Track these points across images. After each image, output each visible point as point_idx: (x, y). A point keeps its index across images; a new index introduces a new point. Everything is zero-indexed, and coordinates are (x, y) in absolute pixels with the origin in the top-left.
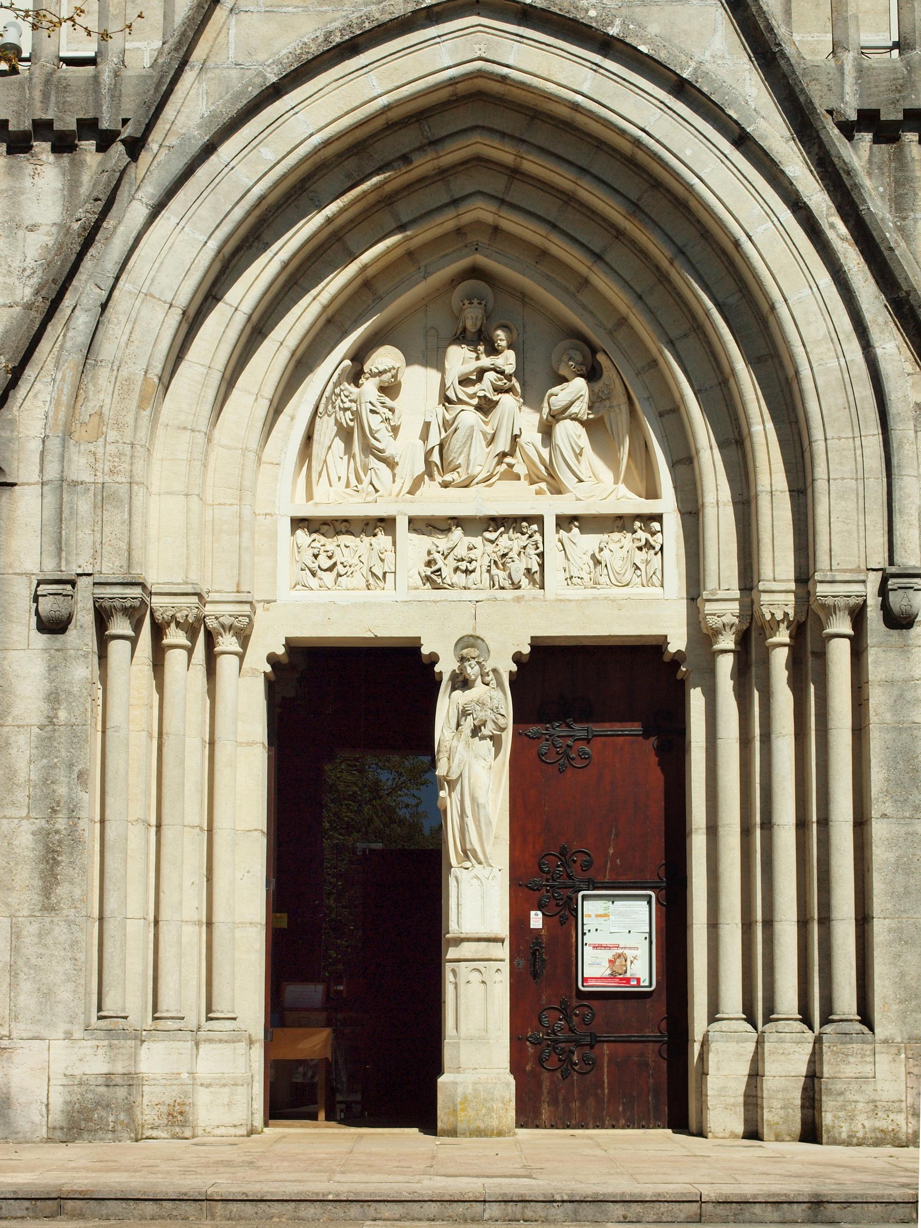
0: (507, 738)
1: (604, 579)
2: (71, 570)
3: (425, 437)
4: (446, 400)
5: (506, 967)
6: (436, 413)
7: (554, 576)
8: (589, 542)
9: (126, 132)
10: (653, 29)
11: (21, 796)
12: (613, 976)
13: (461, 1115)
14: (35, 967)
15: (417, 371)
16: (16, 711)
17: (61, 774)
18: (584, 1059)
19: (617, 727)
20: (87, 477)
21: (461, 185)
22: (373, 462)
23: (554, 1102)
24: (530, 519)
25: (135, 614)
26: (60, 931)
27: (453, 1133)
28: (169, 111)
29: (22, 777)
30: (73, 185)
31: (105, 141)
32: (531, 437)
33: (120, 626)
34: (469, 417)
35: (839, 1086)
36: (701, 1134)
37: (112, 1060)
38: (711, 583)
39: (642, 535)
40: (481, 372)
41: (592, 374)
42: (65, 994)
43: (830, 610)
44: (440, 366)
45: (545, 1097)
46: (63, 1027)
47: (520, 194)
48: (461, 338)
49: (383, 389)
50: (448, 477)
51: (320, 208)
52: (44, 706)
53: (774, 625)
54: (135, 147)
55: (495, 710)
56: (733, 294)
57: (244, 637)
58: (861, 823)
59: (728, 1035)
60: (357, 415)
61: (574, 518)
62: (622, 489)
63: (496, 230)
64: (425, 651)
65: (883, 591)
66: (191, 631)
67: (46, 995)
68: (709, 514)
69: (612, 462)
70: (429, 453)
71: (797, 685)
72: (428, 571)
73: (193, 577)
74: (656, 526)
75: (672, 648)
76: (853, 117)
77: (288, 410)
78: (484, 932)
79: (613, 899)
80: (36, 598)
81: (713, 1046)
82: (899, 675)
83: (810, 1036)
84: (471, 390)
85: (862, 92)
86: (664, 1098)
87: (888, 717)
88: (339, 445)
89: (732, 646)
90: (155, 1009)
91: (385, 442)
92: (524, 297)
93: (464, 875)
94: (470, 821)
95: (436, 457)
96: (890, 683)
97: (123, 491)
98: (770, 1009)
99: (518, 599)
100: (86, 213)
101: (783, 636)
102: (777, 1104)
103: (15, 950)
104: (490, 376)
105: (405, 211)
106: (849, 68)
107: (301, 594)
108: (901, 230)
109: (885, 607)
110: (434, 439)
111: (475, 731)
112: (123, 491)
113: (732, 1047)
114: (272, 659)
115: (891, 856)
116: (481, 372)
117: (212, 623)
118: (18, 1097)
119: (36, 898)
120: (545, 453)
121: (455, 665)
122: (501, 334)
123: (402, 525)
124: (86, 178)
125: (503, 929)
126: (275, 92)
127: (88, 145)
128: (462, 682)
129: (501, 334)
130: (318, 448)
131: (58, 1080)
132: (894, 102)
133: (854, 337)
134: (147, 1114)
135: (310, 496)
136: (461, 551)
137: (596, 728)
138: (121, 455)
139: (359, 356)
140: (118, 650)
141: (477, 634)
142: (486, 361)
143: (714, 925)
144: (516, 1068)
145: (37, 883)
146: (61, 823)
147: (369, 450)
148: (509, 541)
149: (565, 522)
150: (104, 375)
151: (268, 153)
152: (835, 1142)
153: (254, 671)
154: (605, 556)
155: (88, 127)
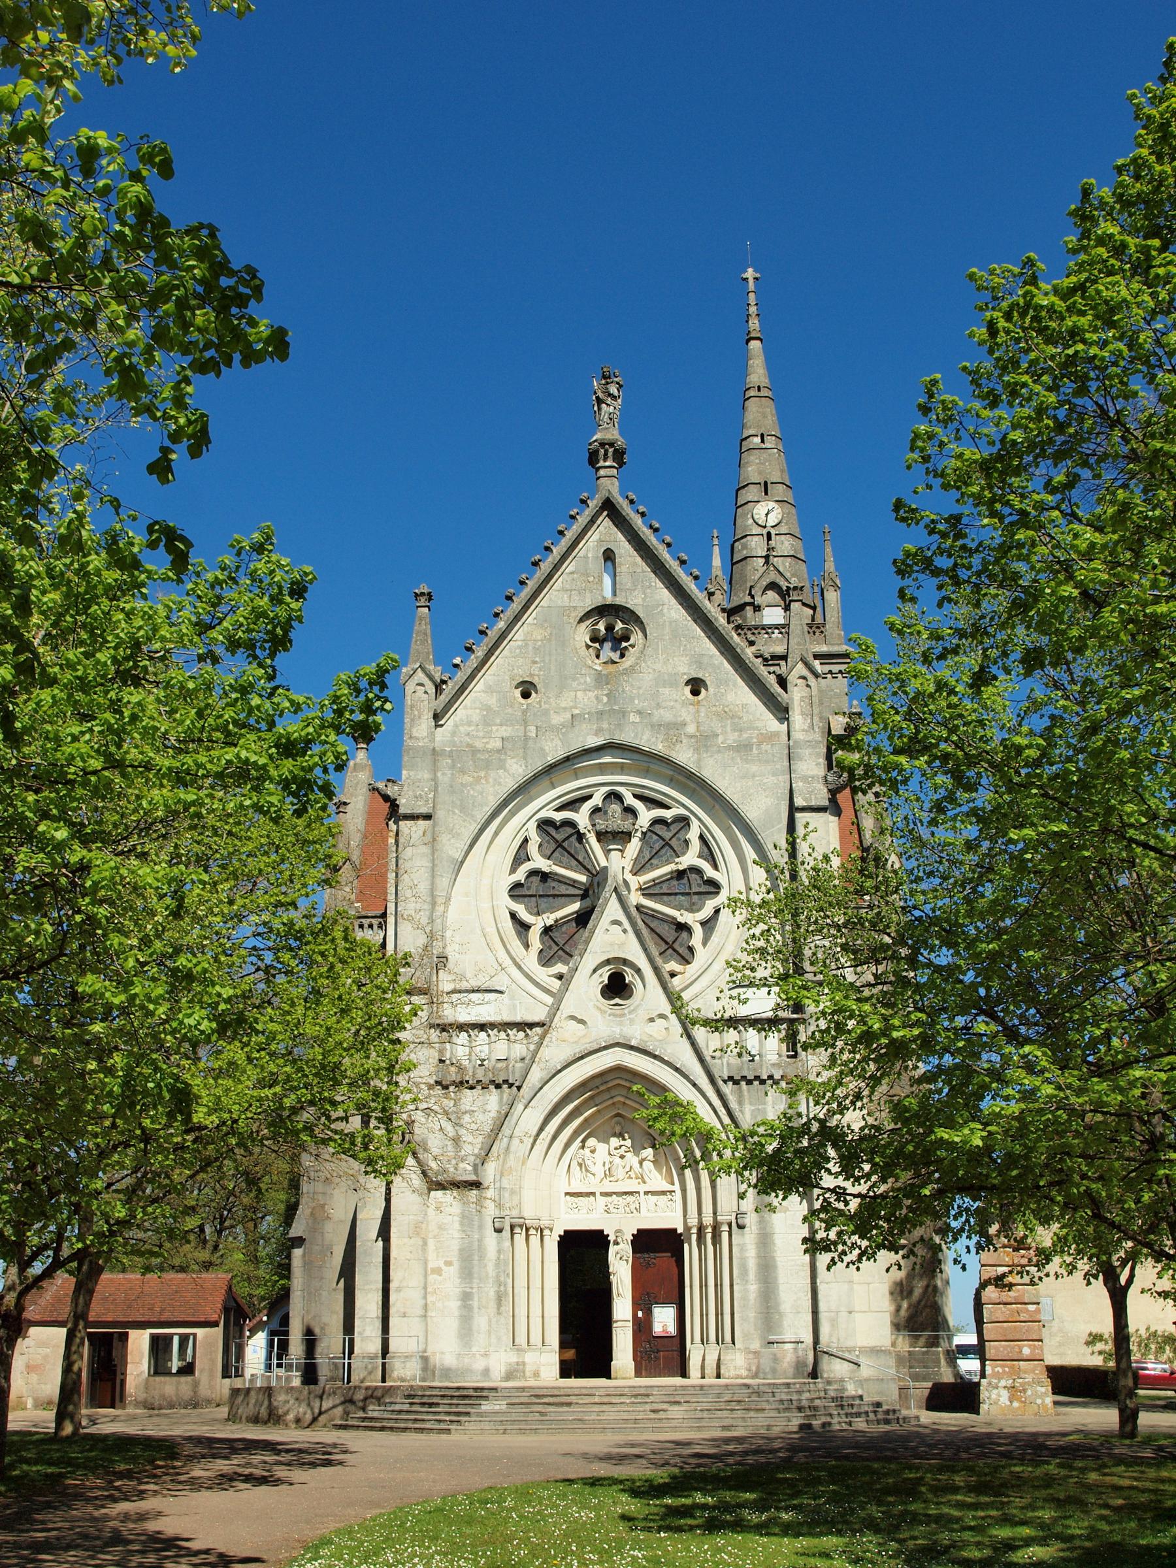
2: (503, 1214)
8: (655, 1198)
21: (613, 1093)
25: (521, 1226)
30: (501, 1099)
32: (636, 1165)
33: (517, 1230)
34: (617, 1160)
41: (653, 1147)
48: (614, 1135)
58: (732, 1286)
67: (499, 1339)
91: (592, 1169)
100: (505, 1108)
105: (598, 1100)
125: (630, 1317)
126: (560, 1071)
128: (616, 1243)
139: (583, 1141)
141: (619, 600)
144: (635, 1359)
148: (629, 1199)
149: (646, 1193)
150: (512, 1156)
151: (558, 1089)
155: (506, 1082)
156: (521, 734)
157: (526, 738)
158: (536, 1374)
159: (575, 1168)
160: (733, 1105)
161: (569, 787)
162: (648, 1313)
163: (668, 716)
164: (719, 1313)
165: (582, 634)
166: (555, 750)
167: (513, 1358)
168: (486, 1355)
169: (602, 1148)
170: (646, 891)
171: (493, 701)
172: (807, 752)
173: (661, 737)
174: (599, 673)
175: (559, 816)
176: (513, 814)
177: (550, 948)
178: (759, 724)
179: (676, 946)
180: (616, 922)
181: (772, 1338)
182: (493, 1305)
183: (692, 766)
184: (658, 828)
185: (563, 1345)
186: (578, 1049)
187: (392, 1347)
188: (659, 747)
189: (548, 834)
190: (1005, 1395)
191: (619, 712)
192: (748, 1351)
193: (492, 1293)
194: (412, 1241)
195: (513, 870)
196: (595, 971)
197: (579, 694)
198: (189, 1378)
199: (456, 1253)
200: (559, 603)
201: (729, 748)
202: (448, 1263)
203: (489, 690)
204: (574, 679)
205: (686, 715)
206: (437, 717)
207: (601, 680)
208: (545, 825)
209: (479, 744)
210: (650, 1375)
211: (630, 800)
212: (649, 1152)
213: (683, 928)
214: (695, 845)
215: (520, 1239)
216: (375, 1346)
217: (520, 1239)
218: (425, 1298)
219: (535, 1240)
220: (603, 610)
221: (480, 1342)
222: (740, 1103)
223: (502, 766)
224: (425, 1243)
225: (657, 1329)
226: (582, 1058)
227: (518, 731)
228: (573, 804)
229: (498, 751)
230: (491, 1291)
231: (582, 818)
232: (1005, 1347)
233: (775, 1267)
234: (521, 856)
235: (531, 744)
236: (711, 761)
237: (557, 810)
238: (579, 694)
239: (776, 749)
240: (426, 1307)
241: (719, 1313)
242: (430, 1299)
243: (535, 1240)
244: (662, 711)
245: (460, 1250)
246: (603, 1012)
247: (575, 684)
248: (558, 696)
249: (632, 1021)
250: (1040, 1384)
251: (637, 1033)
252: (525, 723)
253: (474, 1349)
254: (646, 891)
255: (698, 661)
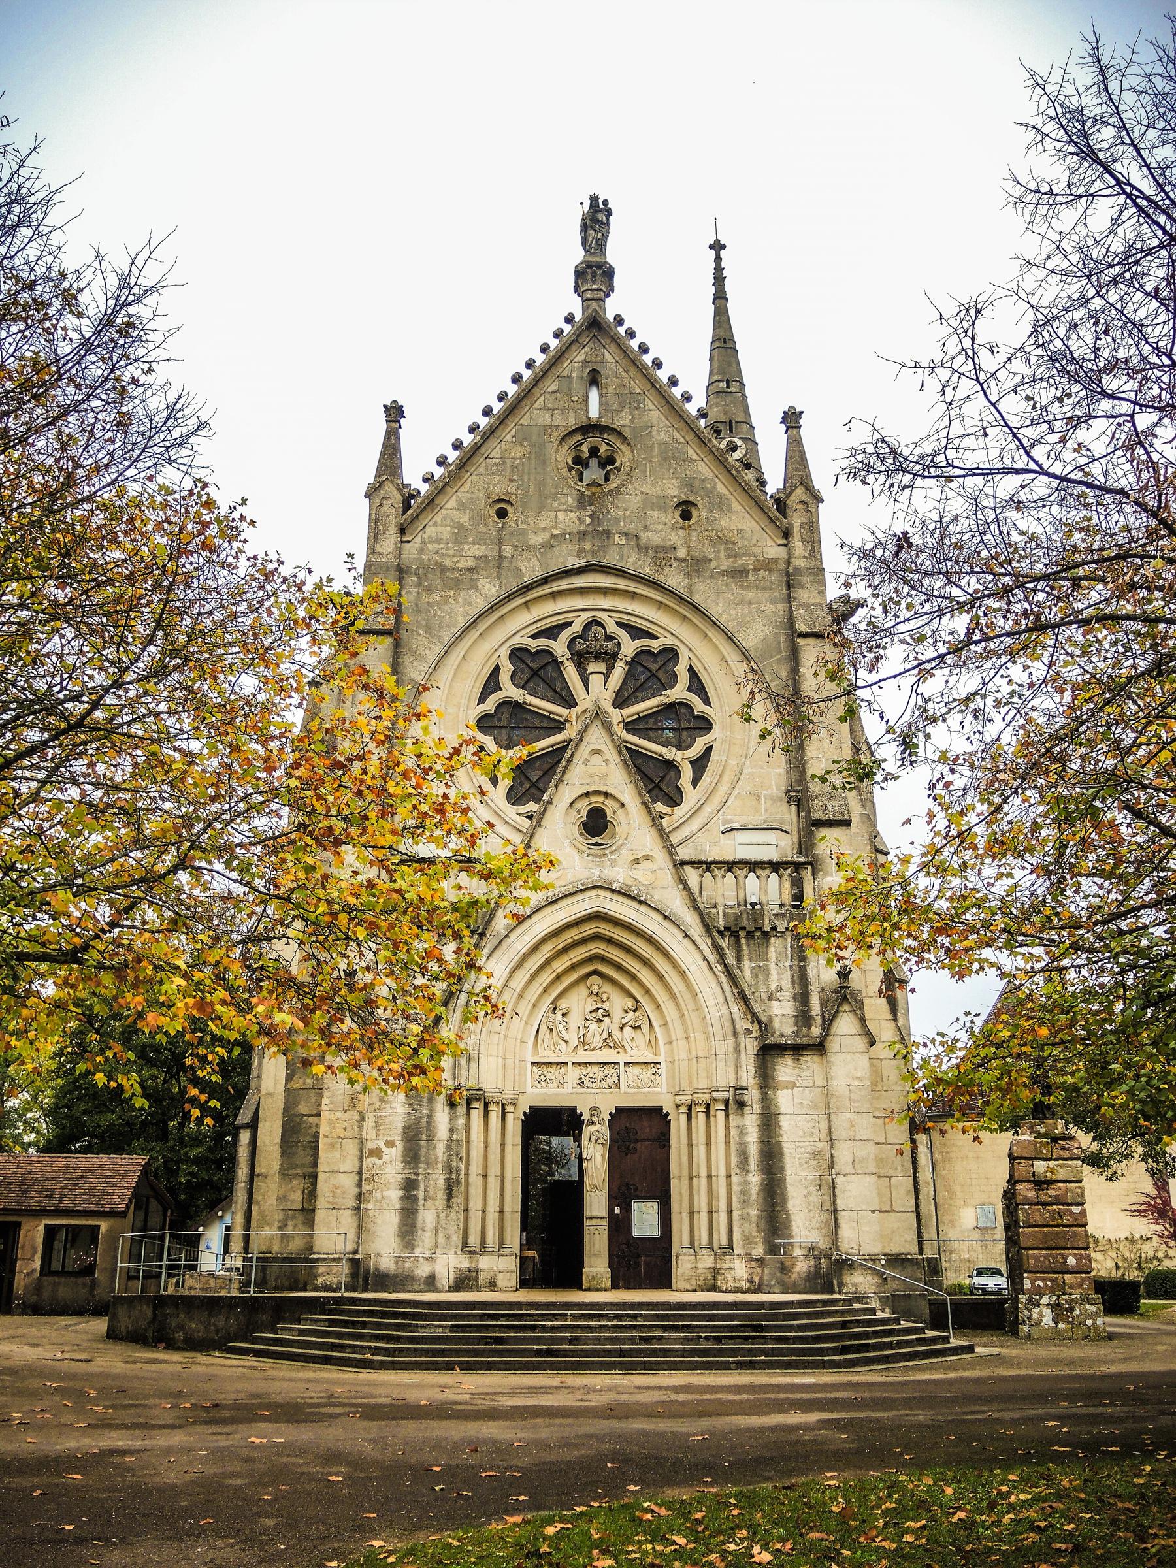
5: (607, 1232)
6: (581, 1024)
11: (440, 1166)
17: (454, 1158)
26: (453, 1215)
34: (593, 1026)
40: (598, 1009)
67: (448, 1238)
73: (499, 1086)
78: (600, 1215)
104: (601, 1011)
107: (533, 1090)
108: (739, 968)
115: (739, 1189)
116: (598, 1009)
123: (570, 1064)
125: (605, 1213)
131: (452, 1269)
133: (425, 1423)
134: (482, 1283)
136: (591, 1075)
146: (454, 1176)
148: (608, 1070)
151: (527, 938)
156: (495, 553)
157: (501, 557)
160: (731, 960)
161: (546, 611)
162: (628, 1210)
163: (656, 540)
165: (564, 456)
166: (531, 569)
167: (465, 1263)
168: (431, 1259)
171: (465, 519)
172: (809, 579)
173: (649, 560)
174: (582, 494)
175: (534, 645)
177: (521, 784)
178: (755, 550)
179: (662, 785)
180: (597, 752)
182: (441, 1195)
184: (643, 659)
185: (527, 1244)
189: (523, 661)
190: (1048, 1315)
191: (602, 533)
192: (749, 1258)
193: (441, 1182)
194: (347, 1116)
195: (482, 700)
196: (571, 804)
197: (560, 514)
198: (88, 1279)
199: (400, 1131)
200: (541, 422)
201: (724, 573)
202: (390, 1144)
204: (555, 499)
205: (676, 538)
206: (402, 531)
207: (583, 501)
208: (518, 654)
209: (448, 563)
210: (628, 1286)
213: (670, 766)
214: (684, 678)
215: (476, 1115)
217: (476, 1115)
218: (359, 1185)
220: (588, 429)
221: (425, 1241)
222: (739, 959)
223: (473, 585)
224: (362, 1118)
227: (491, 550)
228: (552, 632)
229: (470, 570)
230: (439, 1178)
231: (559, 647)
232: (1046, 1257)
234: (491, 684)
235: (506, 563)
236: (703, 587)
237: (533, 637)
238: (560, 514)
239: (775, 576)
240: (360, 1197)
242: (365, 1187)
244: (649, 534)
247: (555, 504)
248: (536, 516)
249: (613, 862)
250: (1089, 1301)
251: (619, 875)
252: (501, 543)
253: (417, 1251)
255: (689, 485)
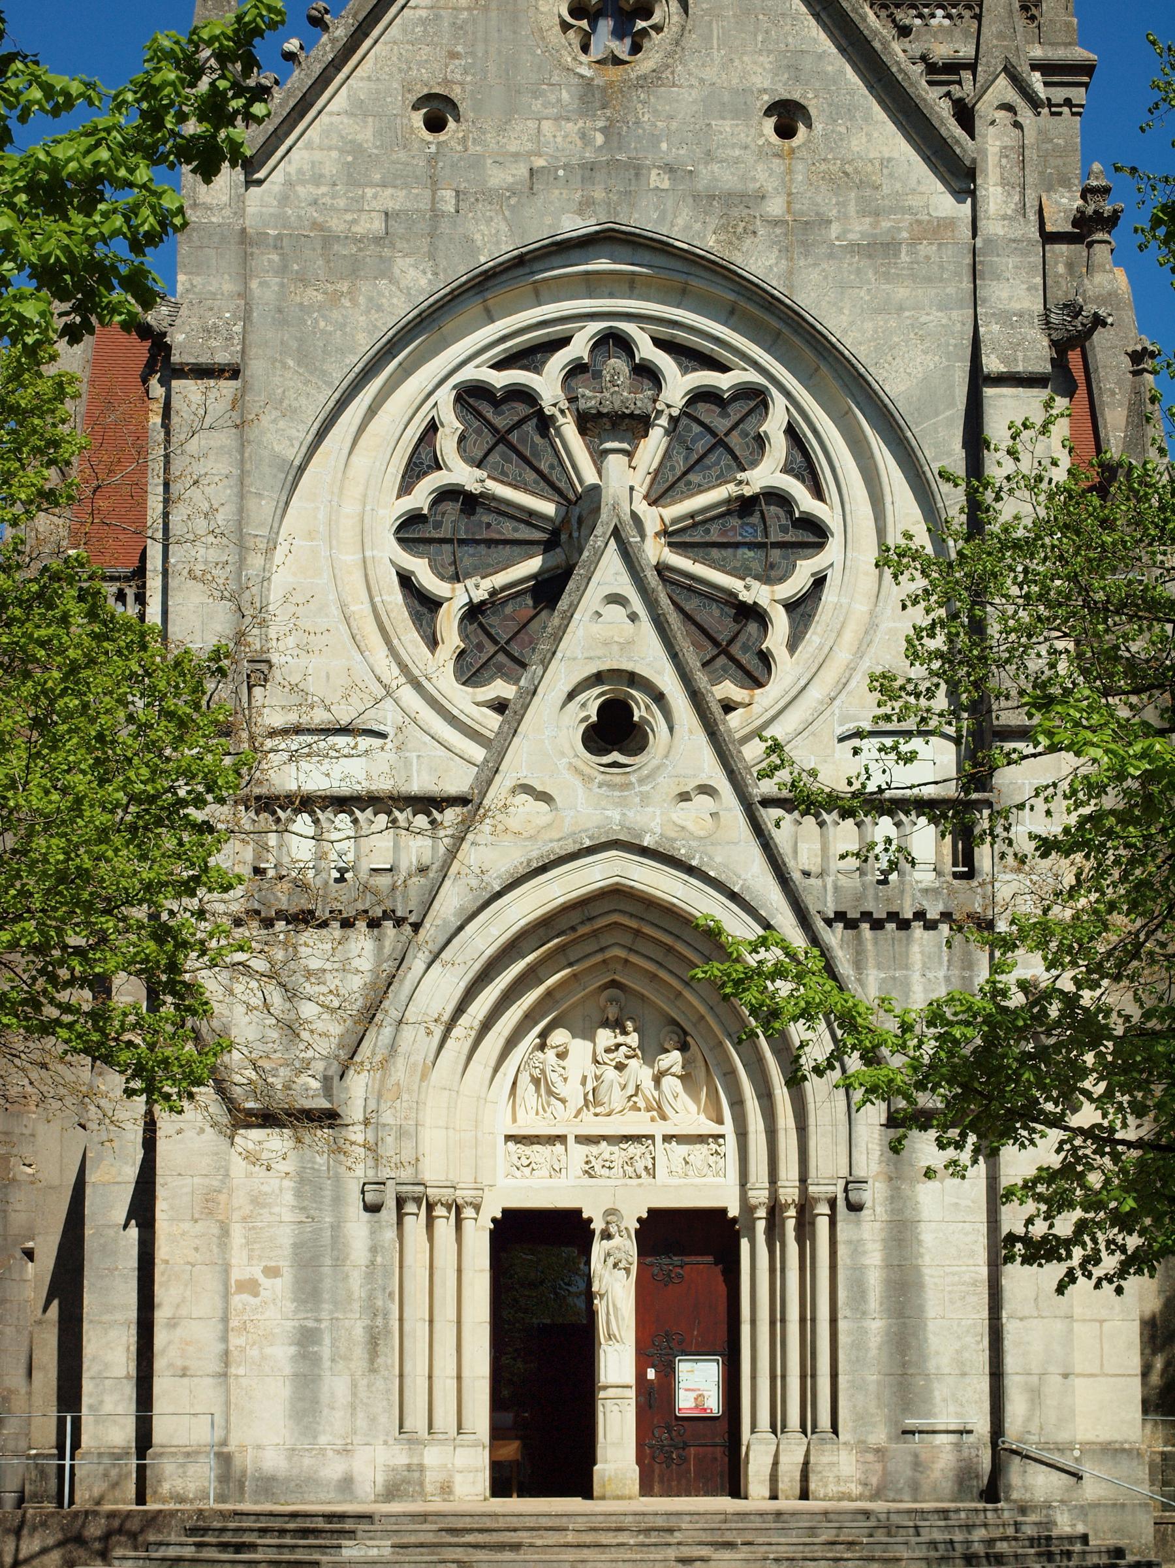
0: (634, 1269)
1: (690, 1173)
3: (584, 1083)
4: (596, 1062)
7: (661, 1170)
9: (413, 919)
10: (718, 859)
11: (356, 1306)
12: (696, 1407)
13: (608, 1488)
14: (366, 1405)
15: (579, 1042)
16: (352, 1257)
17: (379, 1294)
18: (679, 1456)
19: (699, 1259)
20: (391, 1121)
21: (606, 940)
22: (553, 1101)
23: (661, 1481)
24: (647, 1137)
25: (418, 1201)
26: (380, 1384)
27: (603, 1498)
28: (436, 905)
29: (356, 1295)
30: (380, 949)
31: (399, 922)
32: (648, 1084)
33: (410, 1208)
34: (611, 1074)
35: (819, 1468)
36: (746, 1498)
37: (411, 1457)
38: (752, 1178)
39: (714, 1146)
40: (618, 1046)
41: (683, 1048)
42: (383, 1419)
43: (817, 1200)
44: (593, 1040)
45: (656, 1478)
46: (382, 1438)
47: (640, 946)
48: (605, 1024)
49: (559, 1056)
50: (598, 1110)
51: (523, 957)
52: (369, 1255)
53: (787, 1206)
54: (416, 927)
55: (626, 1252)
56: (859, 734)
57: (477, 1208)
58: (833, 1321)
59: (760, 1441)
60: (543, 1071)
61: (673, 1136)
62: (702, 1117)
63: (626, 961)
64: (585, 1215)
65: (846, 1190)
66: (448, 1207)
67: (373, 1419)
68: (752, 1137)
69: (697, 1100)
70: (586, 1095)
71: (800, 1240)
72: (587, 1167)
74: (721, 1141)
75: (731, 1215)
76: (832, 916)
77: (502, 1069)
79: (696, 1361)
80: (363, 1192)
81: (752, 1447)
82: (855, 1238)
83: (805, 1440)
84: (611, 1056)
85: (837, 901)
86: (726, 1479)
87: (848, 1261)
88: (532, 1087)
89: (764, 1215)
90: (401, 1426)
92: (643, 997)
93: (609, 1349)
94: (612, 1318)
95: (590, 1097)
96: (849, 1242)
97: (412, 1129)
98: (784, 1426)
99: (640, 1185)
101: (792, 1212)
102: (786, 1479)
103: (354, 1394)
104: (623, 1049)
106: (830, 887)
107: (510, 1181)
108: (859, 980)
109: (847, 1199)
110: (589, 1087)
111: (615, 1265)
112: (412, 1129)
113: (762, 1448)
114: (494, 1220)
115: (849, 1340)
116: (618, 1046)
117: (460, 1201)
118: (358, 1478)
119: (366, 1365)
120: (656, 1094)
121: (603, 1226)
122: (629, 1024)
123: (571, 1140)
124: (388, 944)
126: (499, 895)
127: (388, 924)
128: (606, 1235)
129: (629, 1024)
130: (519, 1091)
131: (380, 1468)
132: (855, 907)
135: (514, 1120)
136: (606, 1156)
137: (687, 1259)
138: (410, 1108)
139: (543, 1035)
140: (408, 1220)
142: (621, 1039)
143: (754, 1378)
144: (639, 1461)
145: (366, 1356)
146: (379, 1321)
147: (550, 1093)
148: (634, 1149)
149: (667, 1138)
150: (400, 1061)
151: (495, 931)
152: (816, 1499)
153: (483, 1228)
154: (691, 1159)
155: (386, 915)
158: (446, 1489)
159: (526, 1086)
162: (668, 1373)
163: (727, 178)
164: (808, 1374)
167: (400, 1457)
168: (346, 1451)
169: (580, 1049)
170: (675, 537)
174: (588, 83)
175: (500, 379)
176: (406, 371)
177: (480, 647)
181: (911, 1422)
182: (360, 1353)
183: (775, 284)
184: (704, 411)
185: (497, 1433)
186: (536, 853)
187: (160, 1434)
188: (710, 243)
193: (359, 1332)
201: (854, 248)
202: (272, 1272)
203: (359, 110)
204: (536, 94)
205: (765, 176)
211: (646, 350)
212: (673, 1059)
213: (754, 614)
214: (778, 446)
215: (415, 1225)
216: (123, 1434)
217: (415, 1225)
219: (444, 1228)
223: (384, 271)
225: (685, 1402)
226: (543, 869)
233: (920, 1286)
237: (499, 366)
241: (808, 1374)
243: (444, 1228)
245: (295, 1246)
246: (587, 779)
247: (537, 105)
249: (645, 799)
254: (675, 537)
